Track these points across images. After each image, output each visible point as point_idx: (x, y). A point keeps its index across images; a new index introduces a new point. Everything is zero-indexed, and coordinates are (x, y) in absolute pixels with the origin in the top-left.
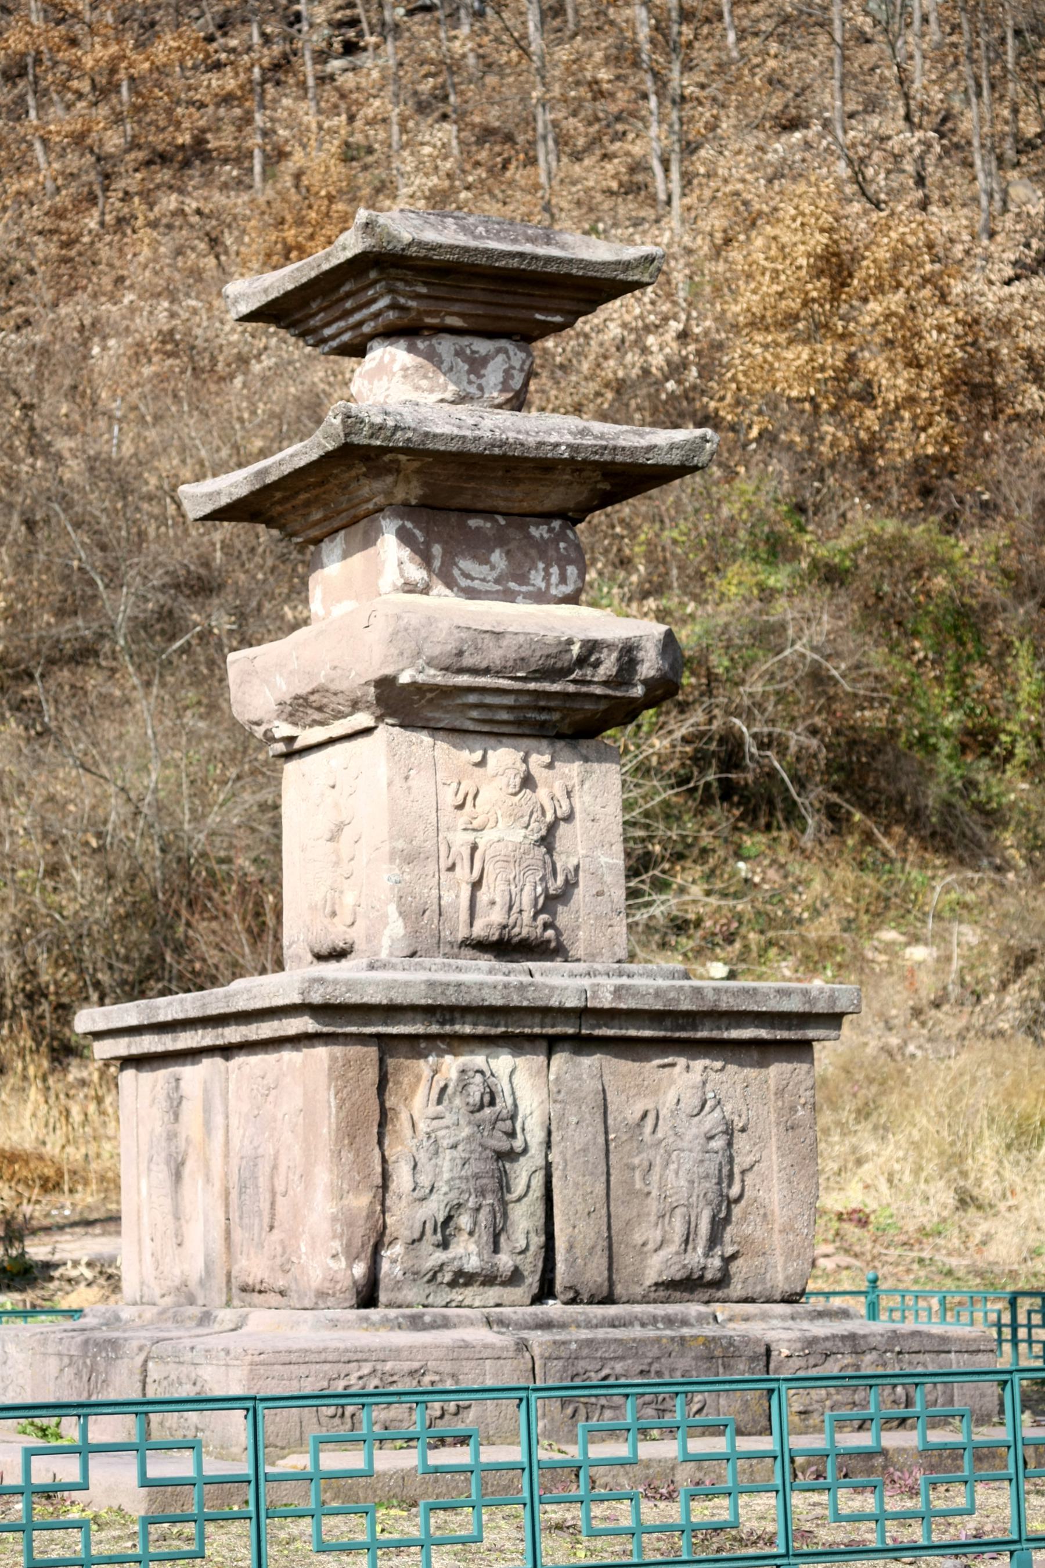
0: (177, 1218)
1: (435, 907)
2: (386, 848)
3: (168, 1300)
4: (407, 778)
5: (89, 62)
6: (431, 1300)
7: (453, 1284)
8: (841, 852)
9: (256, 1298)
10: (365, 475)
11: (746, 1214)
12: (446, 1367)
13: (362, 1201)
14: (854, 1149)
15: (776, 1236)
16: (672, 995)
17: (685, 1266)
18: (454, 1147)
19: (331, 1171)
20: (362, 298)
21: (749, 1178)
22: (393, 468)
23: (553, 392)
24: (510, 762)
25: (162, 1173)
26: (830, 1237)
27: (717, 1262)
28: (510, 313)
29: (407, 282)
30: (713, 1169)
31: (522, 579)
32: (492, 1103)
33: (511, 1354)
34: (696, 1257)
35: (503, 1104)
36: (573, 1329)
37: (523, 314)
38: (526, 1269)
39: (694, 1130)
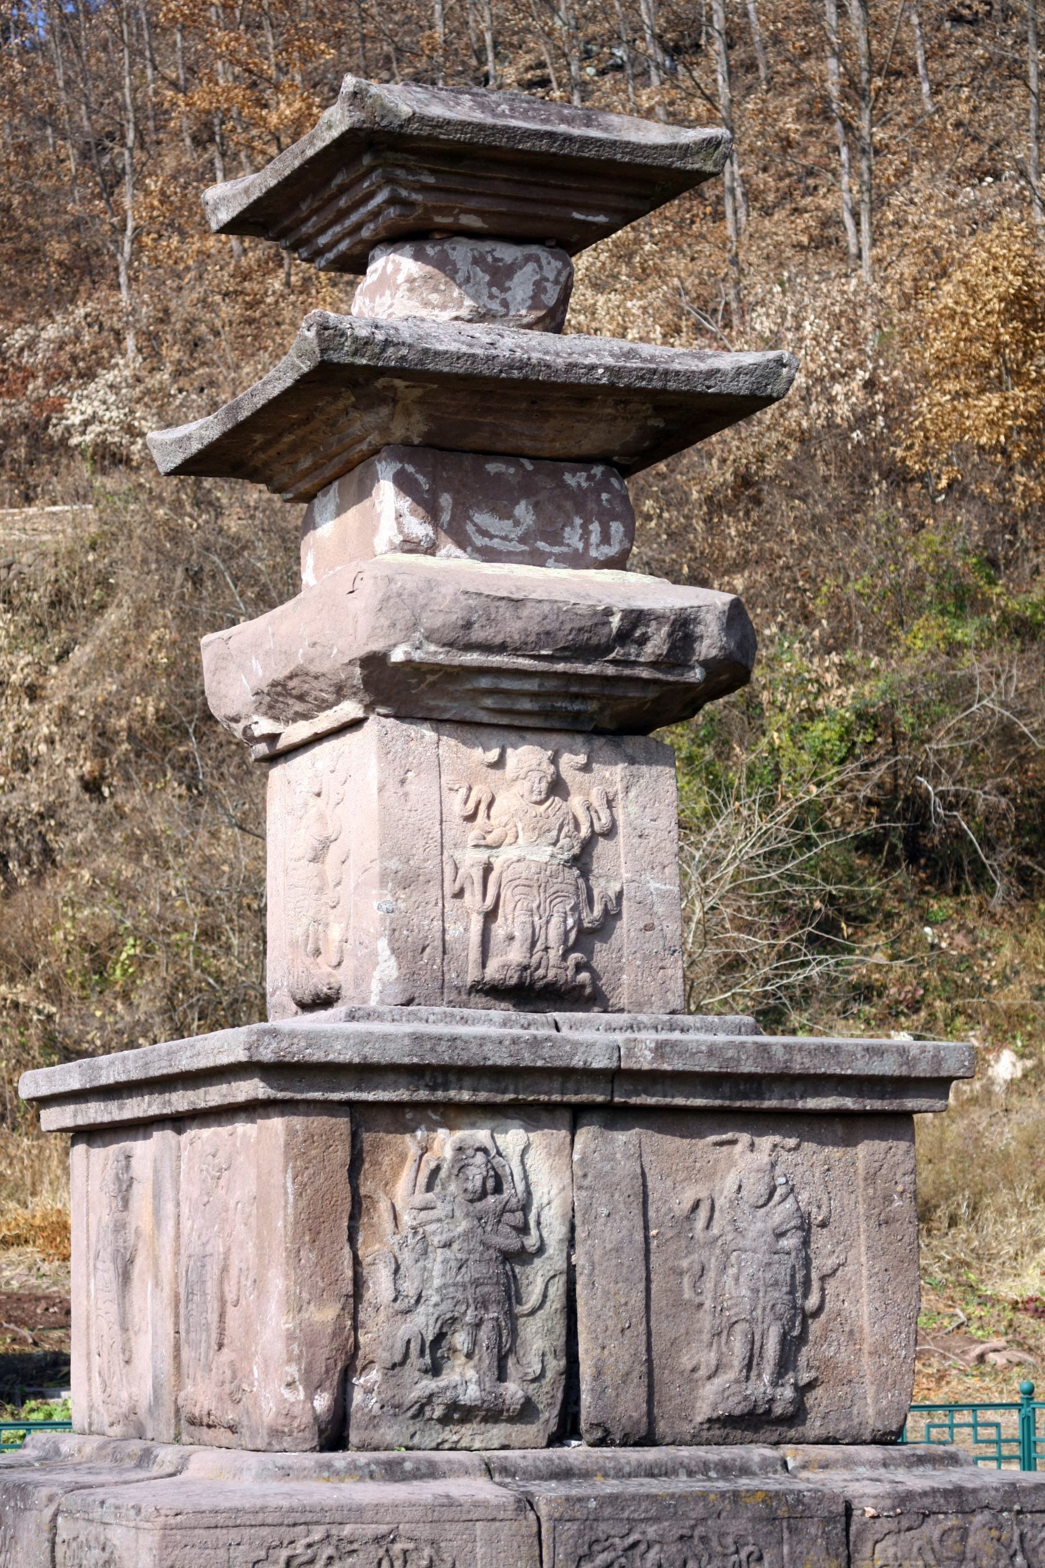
0: (125, 1329)
1: (438, 943)
2: (376, 868)
3: (117, 1431)
4: (403, 782)
5: (274, 119)
6: (416, 1440)
7: (445, 1420)
8: (1032, 918)
9: (206, 1434)
10: (354, 406)
12: (424, 1531)
13: (326, 1315)
14: (1033, 1231)
15: (865, 1359)
16: (730, 1053)
17: (746, 1398)
18: (448, 1245)
19: (287, 1276)
20: (358, 193)
21: (831, 1286)
22: (389, 397)
23: (736, 443)
24: (535, 762)
25: (107, 1273)
26: (1002, 1329)
27: (788, 1393)
28: (541, 211)
29: (409, 170)
30: (784, 1275)
31: (555, 538)
32: (498, 1189)
33: (510, 1514)
34: (761, 1386)
36: (599, 1480)
37: (557, 212)
38: (541, 1401)
39: (759, 1225)
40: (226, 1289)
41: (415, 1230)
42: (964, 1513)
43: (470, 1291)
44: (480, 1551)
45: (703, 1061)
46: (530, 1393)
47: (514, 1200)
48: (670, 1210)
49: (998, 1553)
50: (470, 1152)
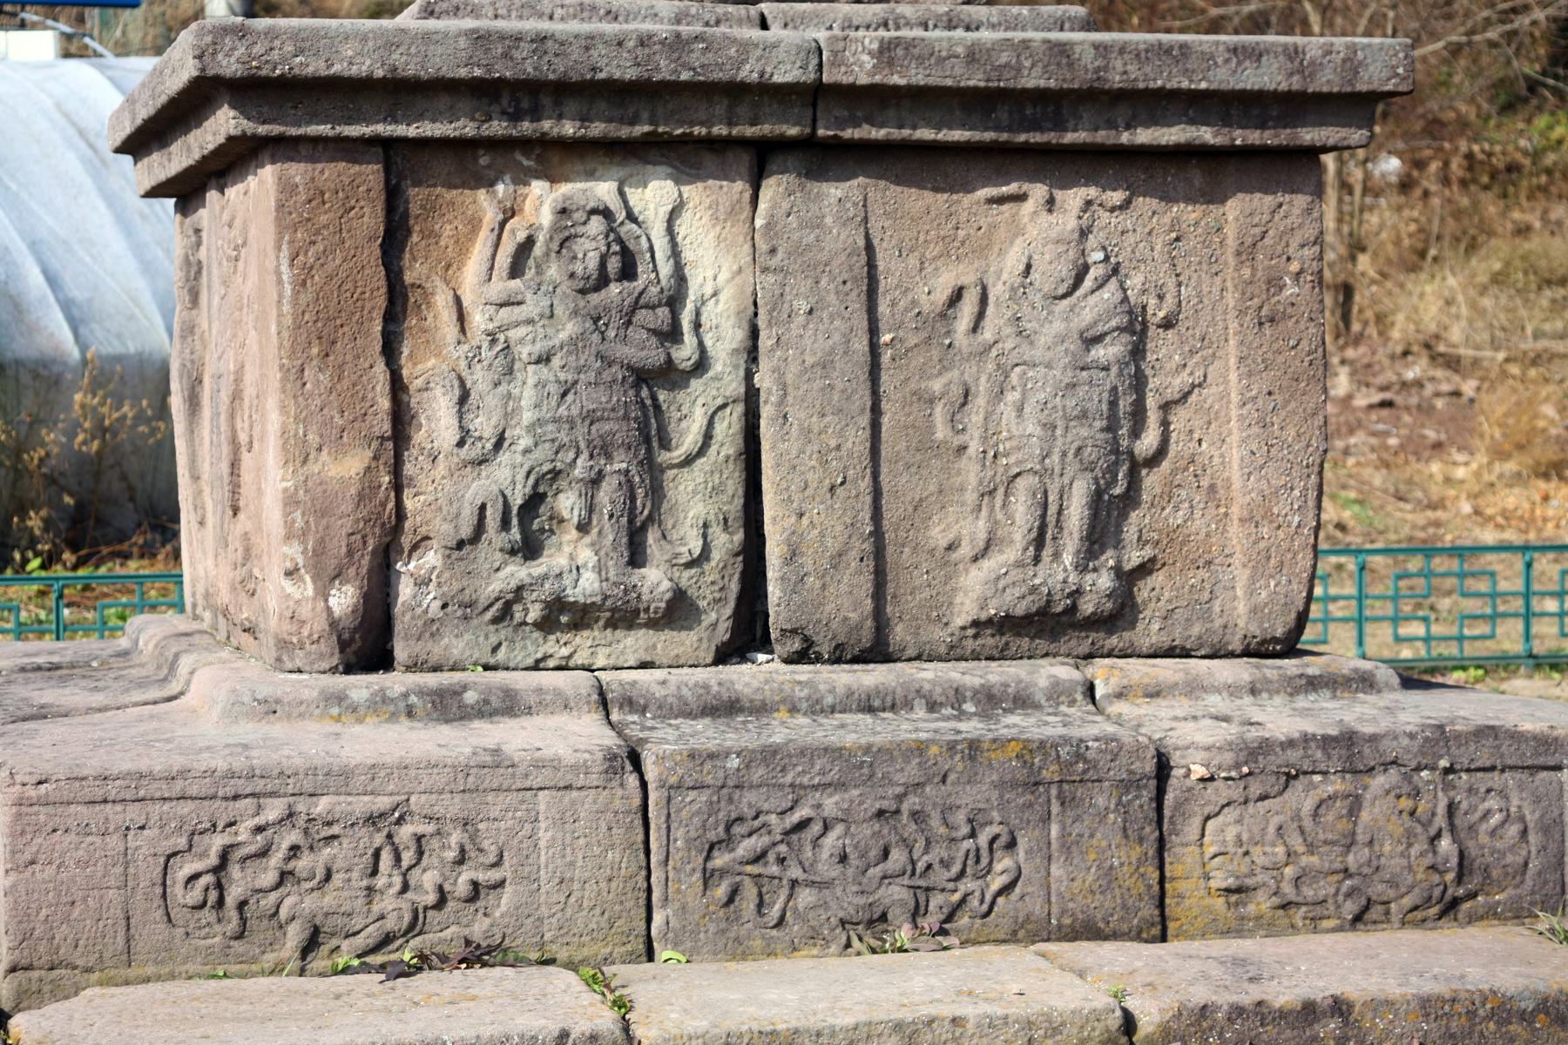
6: (502, 655)
7: (547, 625)
11: (1170, 488)
12: (452, 806)
13: (348, 467)
15: (1234, 529)
16: (1004, 58)
17: (1034, 590)
18: (544, 359)
27: (1105, 581)
32: (628, 272)
33: (594, 779)
34: (1059, 571)
35: (655, 274)
38: (704, 595)
39: (1058, 326)
40: (239, 426)
41: (493, 338)
42: (1355, 772)
43: (581, 432)
44: (544, 837)
45: (958, 71)
46: (684, 583)
47: (654, 290)
48: (914, 303)
49: (1410, 835)
50: (579, 216)
